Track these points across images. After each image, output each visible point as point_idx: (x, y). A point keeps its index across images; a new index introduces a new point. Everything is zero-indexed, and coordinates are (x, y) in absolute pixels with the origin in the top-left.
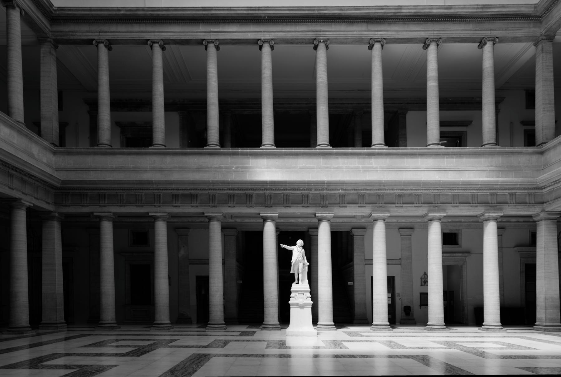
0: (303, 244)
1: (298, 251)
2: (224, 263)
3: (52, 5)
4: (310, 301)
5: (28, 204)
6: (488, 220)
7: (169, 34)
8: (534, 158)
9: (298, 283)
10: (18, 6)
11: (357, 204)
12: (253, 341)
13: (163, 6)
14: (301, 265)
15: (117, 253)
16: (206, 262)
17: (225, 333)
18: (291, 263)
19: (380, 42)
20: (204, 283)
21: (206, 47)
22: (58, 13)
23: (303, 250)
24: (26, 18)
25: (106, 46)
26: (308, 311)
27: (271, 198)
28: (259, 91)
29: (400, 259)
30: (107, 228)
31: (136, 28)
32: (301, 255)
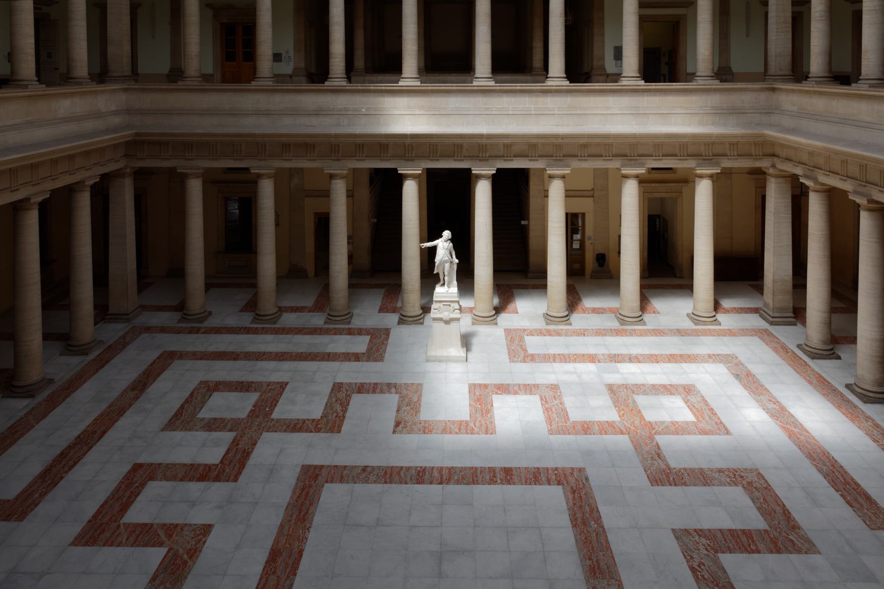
0: (450, 237)
1: (443, 245)
6: (701, 176)
8: (763, 96)
11: (527, 156)
14: (447, 265)
18: (434, 263)
20: (323, 223)
23: (451, 244)
27: (412, 149)
29: (593, 189)
30: (195, 189)
32: (448, 252)
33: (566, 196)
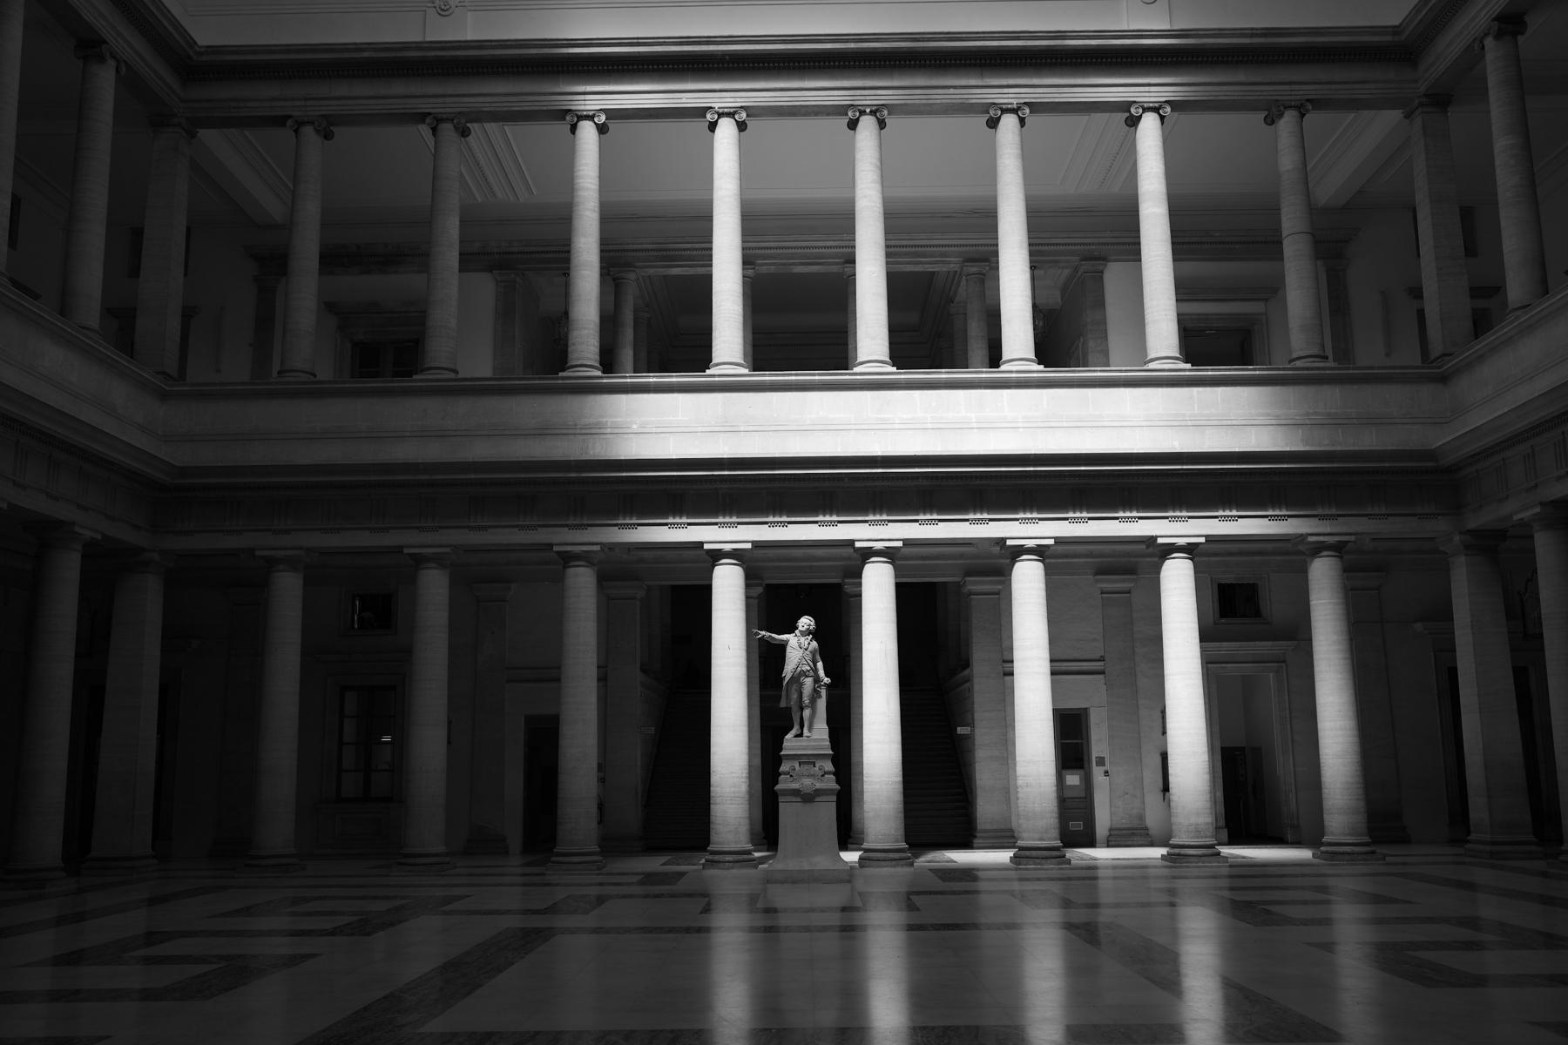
1: (798, 646)
2: (602, 679)
3: (192, 43)
4: (831, 783)
5: (88, 534)
7: (481, 99)
9: (801, 735)
10: (113, 57)
12: (673, 896)
13: (469, 38)
14: (808, 682)
15: (311, 654)
16: (551, 675)
17: (600, 879)
19: (1014, 111)
20: (544, 738)
21: (574, 128)
22: (204, 58)
23: (814, 644)
24: (130, 82)
25: (317, 131)
26: (827, 812)
28: (705, 256)
29: (1102, 659)
30: (288, 591)
31: (399, 87)
33: (1053, 673)
